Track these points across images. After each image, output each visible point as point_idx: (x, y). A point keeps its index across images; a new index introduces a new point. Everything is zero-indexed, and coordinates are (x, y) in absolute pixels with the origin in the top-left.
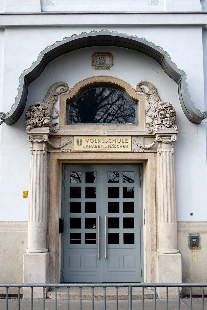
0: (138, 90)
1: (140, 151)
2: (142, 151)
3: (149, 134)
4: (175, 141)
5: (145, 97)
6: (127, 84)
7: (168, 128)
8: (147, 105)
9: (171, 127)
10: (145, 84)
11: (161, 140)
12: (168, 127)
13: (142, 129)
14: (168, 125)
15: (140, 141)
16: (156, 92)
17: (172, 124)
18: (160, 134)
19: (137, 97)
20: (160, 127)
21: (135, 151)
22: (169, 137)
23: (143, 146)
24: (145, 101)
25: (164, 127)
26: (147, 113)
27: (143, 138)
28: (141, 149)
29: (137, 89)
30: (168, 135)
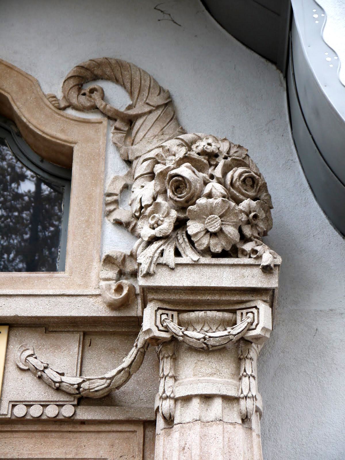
0: (74, 101)
1: (51, 412)
2: (68, 411)
3: (112, 306)
4: (257, 332)
5: (107, 134)
6: (19, 72)
7: (215, 261)
8: (115, 167)
9: (232, 252)
10: (108, 71)
11: (173, 326)
12: (215, 255)
13: (78, 285)
14: (213, 241)
15: (63, 361)
16: (169, 103)
17: (244, 239)
18: (166, 297)
19: (63, 131)
20: (169, 252)
21: (20, 411)
22: (227, 315)
23: (71, 379)
24: (106, 151)
25: (190, 256)
26: (112, 207)
27: (75, 349)
28: (61, 398)
29: (66, 98)
30: (217, 298)
